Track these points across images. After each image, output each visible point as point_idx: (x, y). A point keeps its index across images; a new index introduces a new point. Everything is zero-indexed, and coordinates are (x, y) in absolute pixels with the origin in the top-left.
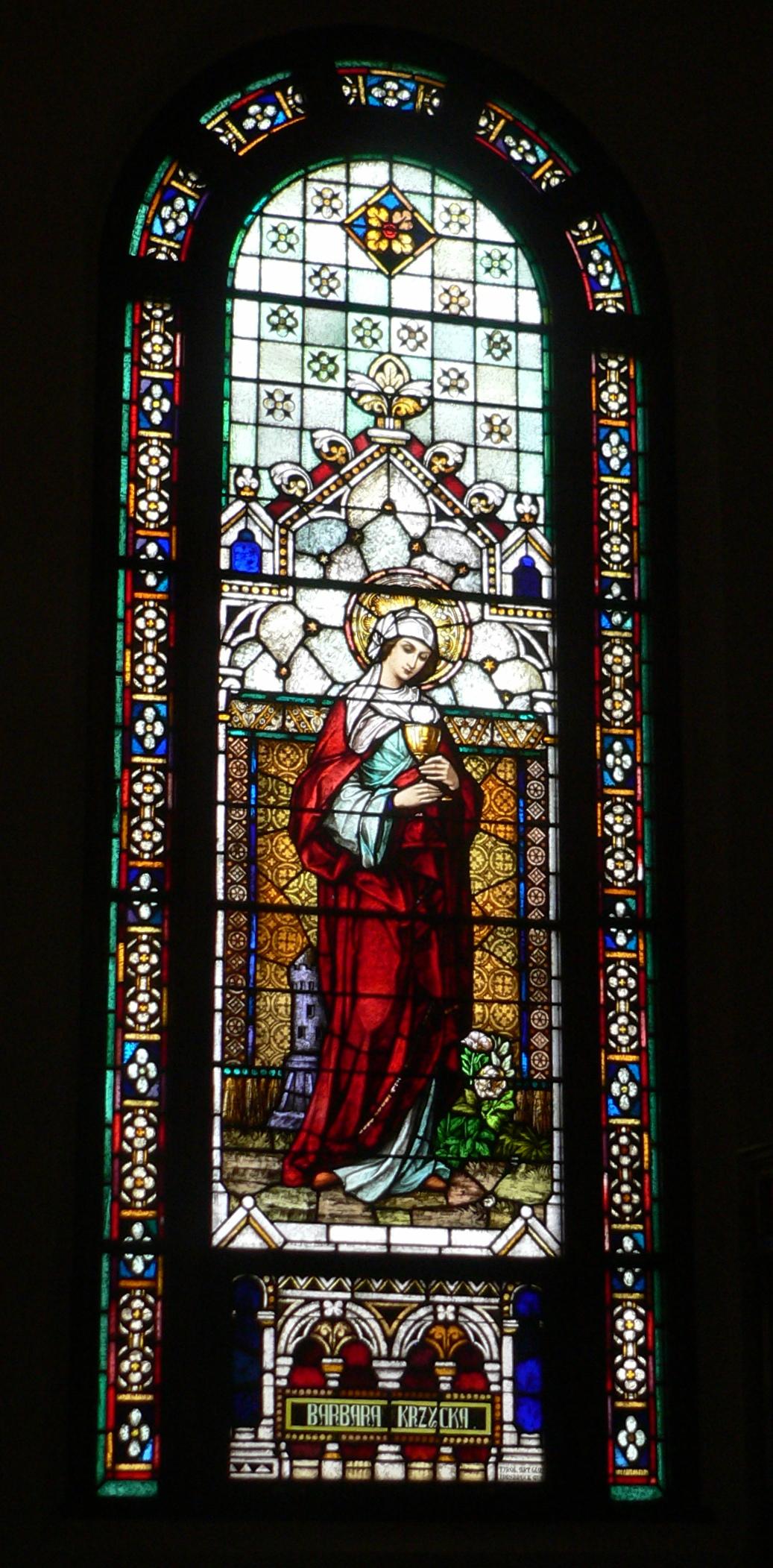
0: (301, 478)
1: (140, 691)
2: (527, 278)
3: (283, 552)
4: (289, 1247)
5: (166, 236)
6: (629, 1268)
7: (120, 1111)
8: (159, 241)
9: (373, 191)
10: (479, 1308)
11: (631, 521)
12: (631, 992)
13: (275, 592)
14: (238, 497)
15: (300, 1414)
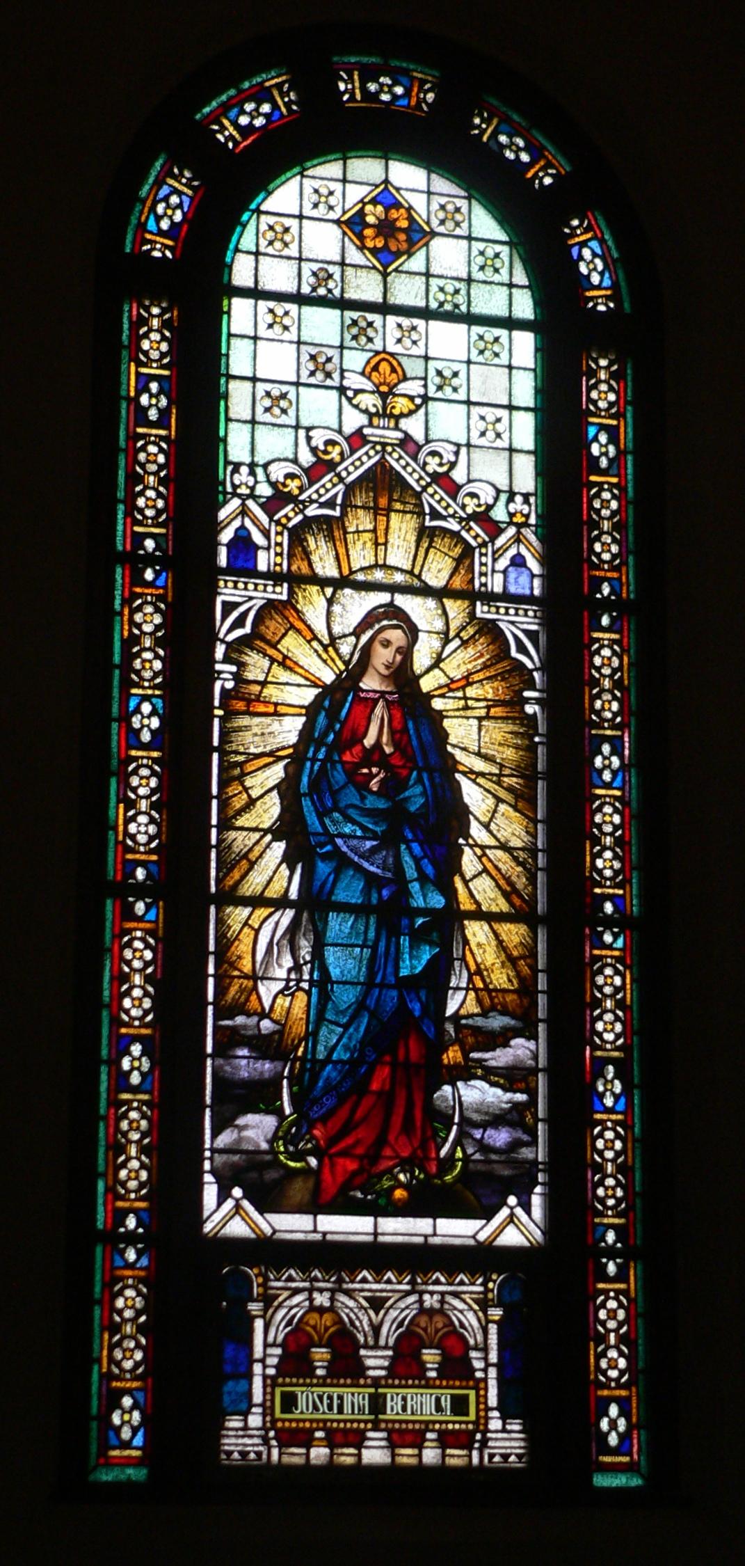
0: (298, 477)
1: (118, 1378)
2: (520, 277)
3: (278, 550)
4: (277, 1235)
5: (161, 233)
6: (611, 1257)
7: (127, 601)
8: (153, 238)
9: (369, 188)
10: (466, 1297)
11: (626, 1160)
12: (616, 828)
14: (234, 494)
15: (290, 1402)
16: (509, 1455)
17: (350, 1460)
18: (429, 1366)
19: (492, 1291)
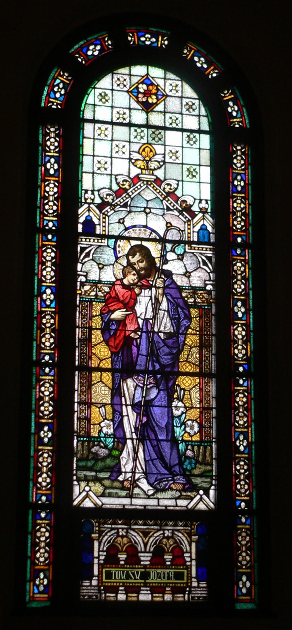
13: (100, 241)
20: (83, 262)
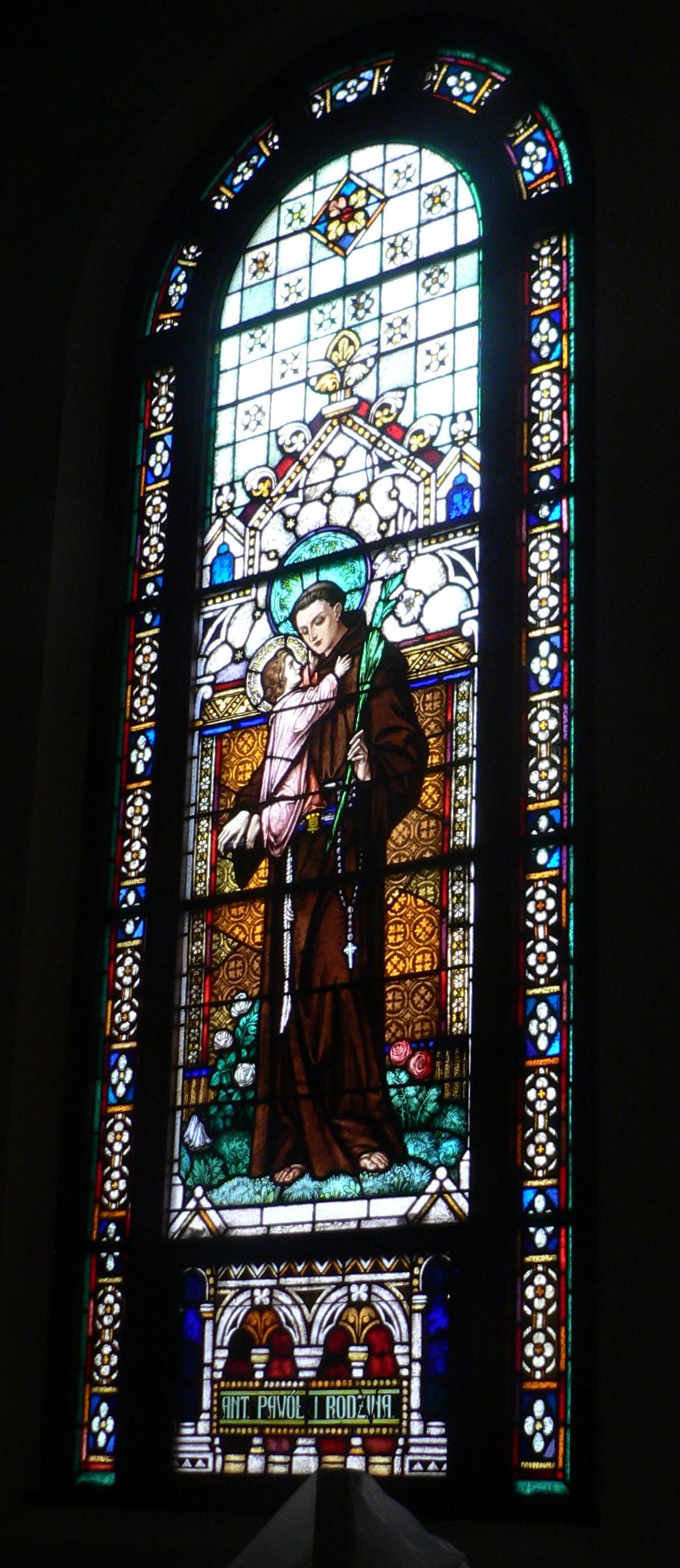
7: (565, 449)
8: (531, 130)
10: (290, 1290)
16: (429, 1462)
17: (280, 1469)
18: (257, 1366)
19: (417, 1276)
20: (207, 653)
